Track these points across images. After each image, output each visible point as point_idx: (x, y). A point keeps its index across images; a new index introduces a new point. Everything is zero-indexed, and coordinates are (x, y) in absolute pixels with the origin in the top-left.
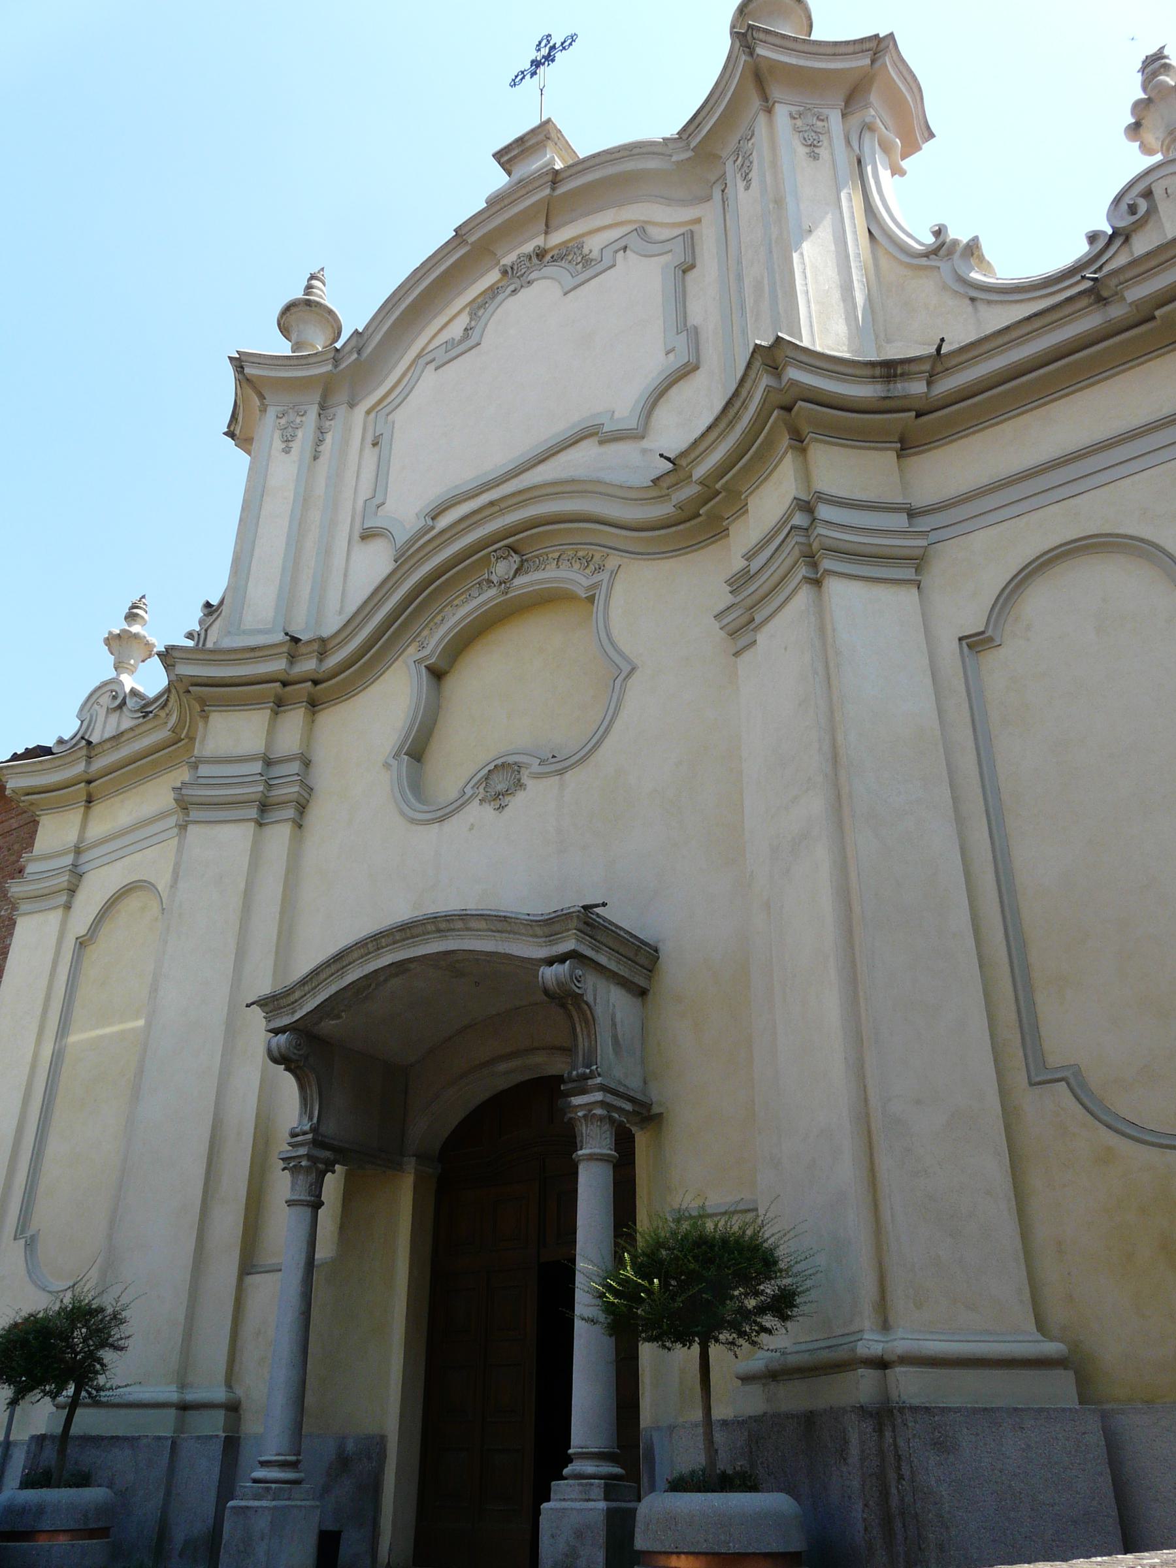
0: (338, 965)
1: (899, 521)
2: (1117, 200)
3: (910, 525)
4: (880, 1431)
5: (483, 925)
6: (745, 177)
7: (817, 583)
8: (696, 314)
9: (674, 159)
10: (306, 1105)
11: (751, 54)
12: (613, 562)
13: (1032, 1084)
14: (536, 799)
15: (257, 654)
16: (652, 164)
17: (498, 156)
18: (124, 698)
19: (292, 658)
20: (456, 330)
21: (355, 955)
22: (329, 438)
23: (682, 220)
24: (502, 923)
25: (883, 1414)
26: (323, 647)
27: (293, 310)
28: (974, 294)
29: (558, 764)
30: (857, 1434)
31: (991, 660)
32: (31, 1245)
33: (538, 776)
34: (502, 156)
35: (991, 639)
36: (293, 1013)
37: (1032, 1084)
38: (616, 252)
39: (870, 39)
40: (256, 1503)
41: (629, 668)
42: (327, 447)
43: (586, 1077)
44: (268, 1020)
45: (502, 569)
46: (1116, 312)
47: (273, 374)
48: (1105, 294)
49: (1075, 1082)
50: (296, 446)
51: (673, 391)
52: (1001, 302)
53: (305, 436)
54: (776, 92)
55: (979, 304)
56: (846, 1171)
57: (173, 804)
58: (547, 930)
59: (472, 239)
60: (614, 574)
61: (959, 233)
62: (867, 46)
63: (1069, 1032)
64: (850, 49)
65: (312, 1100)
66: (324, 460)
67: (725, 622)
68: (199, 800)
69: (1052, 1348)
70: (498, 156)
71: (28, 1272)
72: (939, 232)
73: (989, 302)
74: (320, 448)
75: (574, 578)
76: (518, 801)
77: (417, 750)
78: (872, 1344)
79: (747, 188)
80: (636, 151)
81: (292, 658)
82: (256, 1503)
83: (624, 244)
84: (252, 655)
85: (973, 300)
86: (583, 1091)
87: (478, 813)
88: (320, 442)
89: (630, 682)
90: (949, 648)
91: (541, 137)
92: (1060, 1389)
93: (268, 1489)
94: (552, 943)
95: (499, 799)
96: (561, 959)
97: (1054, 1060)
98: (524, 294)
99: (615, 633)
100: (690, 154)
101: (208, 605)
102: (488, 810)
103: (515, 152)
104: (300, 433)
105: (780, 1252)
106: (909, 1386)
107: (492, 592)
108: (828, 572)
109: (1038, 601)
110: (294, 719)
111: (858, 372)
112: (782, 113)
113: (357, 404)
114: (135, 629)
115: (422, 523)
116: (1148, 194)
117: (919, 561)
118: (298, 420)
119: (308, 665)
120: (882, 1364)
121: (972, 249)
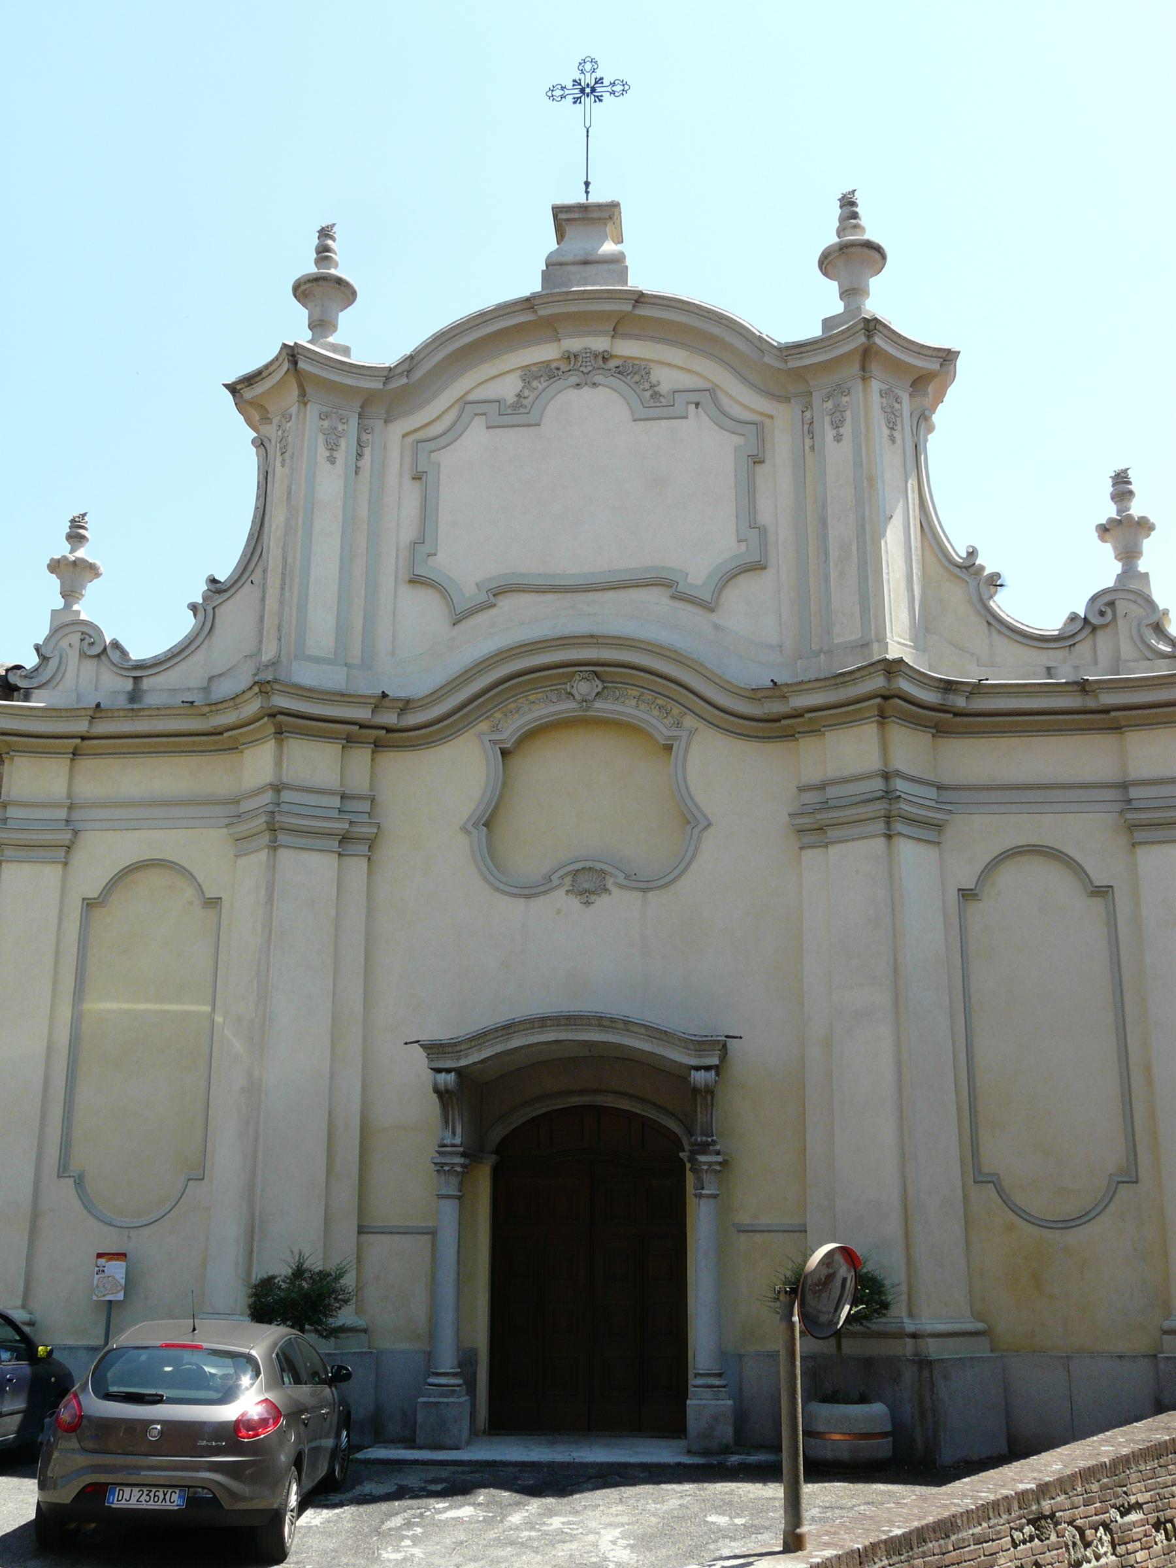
0: (504, 1032)
1: (932, 793)
2: (1094, 599)
3: (939, 796)
4: (920, 1371)
5: (643, 1031)
6: (837, 426)
7: (889, 837)
8: (765, 517)
9: (766, 359)
10: (447, 1122)
11: (869, 337)
12: (690, 721)
13: (975, 1182)
14: (618, 905)
15: (345, 699)
16: (741, 345)
17: (557, 211)
18: (105, 649)
19: (376, 709)
20: (508, 388)
21: (521, 1027)
22: (367, 452)
23: (752, 406)
24: (662, 1035)
25: (924, 1363)
26: (406, 706)
27: (321, 283)
28: (992, 621)
29: (644, 884)
30: (909, 1374)
31: (973, 908)
32: (80, 1183)
33: (621, 886)
34: (561, 212)
35: (976, 895)
36: (458, 1059)
37: (975, 1182)
38: (688, 403)
39: (945, 350)
40: (446, 1400)
41: (706, 823)
42: (366, 462)
43: (708, 1144)
44: (431, 1060)
45: (583, 688)
46: (1091, 703)
47: (324, 374)
48: (1087, 688)
49: (995, 1181)
50: (340, 455)
51: (741, 578)
52: (1008, 637)
53: (347, 446)
54: (875, 368)
55: (993, 629)
56: (892, 1228)
57: (264, 827)
58: (697, 1047)
59: (542, 312)
60: (692, 733)
61: (988, 562)
62: (940, 354)
63: (999, 1154)
64: (929, 353)
65: (453, 1118)
66: (365, 474)
67: (798, 821)
68: (289, 827)
69: (980, 1326)
70: (557, 211)
71: (86, 1207)
72: (972, 554)
73: (1000, 632)
74: (360, 464)
75: (661, 728)
76: (602, 902)
77: (488, 821)
78: (910, 1327)
79: (838, 438)
80: (723, 321)
81: (376, 709)
82: (446, 1400)
83: (697, 400)
84: (342, 699)
85: (989, 624)
86: (705, 1153)
87: (562, 900)
88: (359, 455)
89: (706, 834)
90: (953, 895)
91: (606, 215)
92: (980, 1348)
93: (453, 1391)
94: (700, 1056)
95: (587, 895)
96: (707, 1068)
97: (985, 1170)
98: (586, 391)
99: (692, 787)
100: (781, 365)
101: (213, 581)
102: (574, 903)
103: (576, 216)
104: (343, 442)
105: (886, 1282)
106: (933, 1349)
107: (572, 705)
108: (900, 834)
109: (1008, 875)
110: (361, 756)
111: (931, 683)
112: (876, 386)
113: (391, 421)
114: (81, 553)
115: (483, 597)
116: (1111, 604)
117: (938, 826)
118: (340, 427)
119: (390, 718)
120: (914, 1336)
121: (994, 582)
